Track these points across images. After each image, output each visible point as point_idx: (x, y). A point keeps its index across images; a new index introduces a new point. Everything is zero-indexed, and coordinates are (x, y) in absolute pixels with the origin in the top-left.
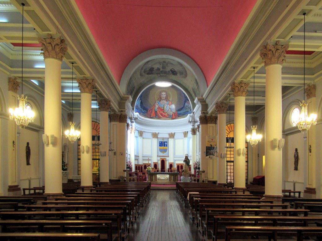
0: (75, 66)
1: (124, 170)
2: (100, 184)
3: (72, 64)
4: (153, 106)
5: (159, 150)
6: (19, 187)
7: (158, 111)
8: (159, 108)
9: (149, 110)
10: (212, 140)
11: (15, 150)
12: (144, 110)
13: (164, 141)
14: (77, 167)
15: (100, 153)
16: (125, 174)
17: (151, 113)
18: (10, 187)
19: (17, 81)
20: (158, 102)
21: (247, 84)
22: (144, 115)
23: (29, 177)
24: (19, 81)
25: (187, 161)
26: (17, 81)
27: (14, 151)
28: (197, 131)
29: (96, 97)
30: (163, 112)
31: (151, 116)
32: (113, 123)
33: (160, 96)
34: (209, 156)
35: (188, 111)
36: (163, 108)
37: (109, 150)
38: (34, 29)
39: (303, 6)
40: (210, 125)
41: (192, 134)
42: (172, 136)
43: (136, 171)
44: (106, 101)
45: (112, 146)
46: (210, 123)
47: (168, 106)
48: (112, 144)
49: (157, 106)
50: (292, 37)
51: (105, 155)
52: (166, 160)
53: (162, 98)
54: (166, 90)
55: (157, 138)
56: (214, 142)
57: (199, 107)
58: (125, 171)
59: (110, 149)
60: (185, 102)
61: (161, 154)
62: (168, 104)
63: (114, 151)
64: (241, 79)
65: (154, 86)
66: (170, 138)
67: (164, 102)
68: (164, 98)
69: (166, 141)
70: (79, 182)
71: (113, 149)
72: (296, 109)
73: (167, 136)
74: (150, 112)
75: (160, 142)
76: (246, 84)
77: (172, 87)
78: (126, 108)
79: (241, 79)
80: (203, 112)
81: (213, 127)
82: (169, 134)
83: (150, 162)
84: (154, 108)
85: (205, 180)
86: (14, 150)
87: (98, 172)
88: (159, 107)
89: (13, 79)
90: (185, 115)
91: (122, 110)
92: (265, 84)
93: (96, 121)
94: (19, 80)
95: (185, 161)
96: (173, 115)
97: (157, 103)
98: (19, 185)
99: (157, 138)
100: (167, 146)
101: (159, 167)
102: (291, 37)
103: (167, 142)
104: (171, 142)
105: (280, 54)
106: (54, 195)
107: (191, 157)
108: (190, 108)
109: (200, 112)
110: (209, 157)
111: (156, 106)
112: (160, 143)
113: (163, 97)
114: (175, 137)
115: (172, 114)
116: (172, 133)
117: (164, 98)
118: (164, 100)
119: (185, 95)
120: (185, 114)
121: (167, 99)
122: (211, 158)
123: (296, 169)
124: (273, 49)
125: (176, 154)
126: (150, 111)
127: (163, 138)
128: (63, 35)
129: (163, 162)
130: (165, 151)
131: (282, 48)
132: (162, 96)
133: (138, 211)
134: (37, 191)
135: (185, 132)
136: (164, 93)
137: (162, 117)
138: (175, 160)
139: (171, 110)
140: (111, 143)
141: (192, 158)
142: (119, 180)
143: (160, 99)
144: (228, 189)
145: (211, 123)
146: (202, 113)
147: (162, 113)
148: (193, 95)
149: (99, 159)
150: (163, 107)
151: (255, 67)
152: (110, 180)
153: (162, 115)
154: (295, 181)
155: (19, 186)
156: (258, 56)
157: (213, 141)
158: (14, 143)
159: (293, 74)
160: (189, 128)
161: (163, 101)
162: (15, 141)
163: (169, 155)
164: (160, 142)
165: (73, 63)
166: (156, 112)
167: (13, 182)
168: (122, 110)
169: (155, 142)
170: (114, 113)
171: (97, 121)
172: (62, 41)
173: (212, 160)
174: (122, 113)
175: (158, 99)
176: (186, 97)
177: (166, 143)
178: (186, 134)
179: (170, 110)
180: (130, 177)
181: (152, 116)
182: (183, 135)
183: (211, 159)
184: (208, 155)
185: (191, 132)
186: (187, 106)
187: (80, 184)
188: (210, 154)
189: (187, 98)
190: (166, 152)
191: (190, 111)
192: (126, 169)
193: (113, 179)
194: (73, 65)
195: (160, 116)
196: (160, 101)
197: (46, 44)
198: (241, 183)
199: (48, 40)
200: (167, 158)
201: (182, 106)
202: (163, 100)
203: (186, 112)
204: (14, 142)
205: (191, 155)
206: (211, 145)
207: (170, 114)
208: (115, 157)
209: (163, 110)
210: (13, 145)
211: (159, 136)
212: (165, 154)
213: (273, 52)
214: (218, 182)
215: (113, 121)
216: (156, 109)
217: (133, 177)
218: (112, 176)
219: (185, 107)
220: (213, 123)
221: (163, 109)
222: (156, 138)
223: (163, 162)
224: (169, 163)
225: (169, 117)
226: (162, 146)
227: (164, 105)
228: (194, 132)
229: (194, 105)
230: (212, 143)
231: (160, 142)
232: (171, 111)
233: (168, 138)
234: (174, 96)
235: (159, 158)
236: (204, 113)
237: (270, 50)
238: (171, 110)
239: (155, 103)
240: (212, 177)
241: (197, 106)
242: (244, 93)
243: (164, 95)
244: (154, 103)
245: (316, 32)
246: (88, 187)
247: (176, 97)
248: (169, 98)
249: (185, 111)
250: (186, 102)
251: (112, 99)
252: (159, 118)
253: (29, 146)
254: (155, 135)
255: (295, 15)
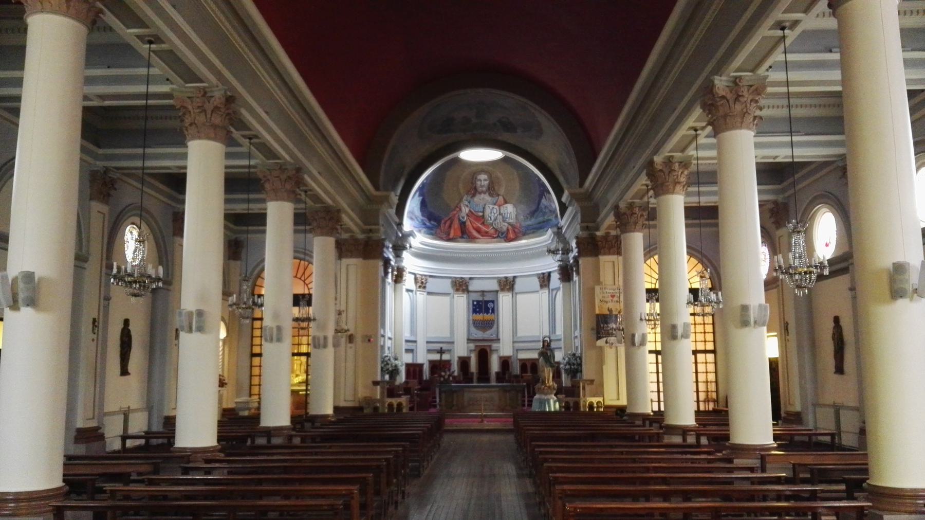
0: (256, 143)
1: (375, 380)
2: (313, 419)
3: (248, 140)
4: (454, 210)
5: (471, 322)
6: (99, 431)
7: (468, 223)
8: (471, 214)
9: (443, 222)
10: (613, 296)
11: (97, 343)
12: (430, 220)
13: (486, 299)
14: (247, 376)
15: (310, 338)
16: (378, 392)
17: (450, 227)
18: (79, 431)
19: (110, 177)
20: (469, 198)
21: (685, 164)
22: (432, 234)
23: (125, 406)
24: (115, 177)
25: (547, 353)
26: (110, 175)
27: (95, 341)
28: (574, 273)
29: (306, 203)
30: (483, 223)
31: (449, 235)
32: (345, 261)
33: (472, 183)
34: (605, 339)
35: (551, 220)
36: (481, 214)
37: (337, 331)
38: (168, 80)
39: (778, 14)
40: (606, 260)
41: (560, 279)
42: (508, 284)
43: (406, 382)
44: (329, 211)
45: (344, 320)
46: (605, 254)
47: (496, 207)
48: (344, 315)
49: (465, 210)
50: (770, 67)
51: (325, 346)
52: (491, 351)
53: (480, 189)
54: (490, 168)
55: (468, 291)
56: (617, 301)
57: (576, 213)
58: (376, 383)
59: (339, 328)
60: (541, 196)
61: (478, 334)
62: (495, 204)
63: (349, 333)
64: (670, 151)
65: (457, 161)
66: (502, 290)
67: (483, 199)
68: (484, 189)
69: (491, 299)
70: (256, 418)
71: (346, 328)
72: (826, 214)
73: (494, 286)
74: (447, 224)
75: (473, 301)
76: (683, 164)
77: (505, 160)
78: (381, 222)
79: (670, 151)
80: (586, 224)
81: (614, 262)
82: (500, 281)
83: (446, 357)
84: (457, 215)
85: (595, 405)
86: (93, 340)
87: (304, 388)
88: (470, 211)
89: (102, 172)
90: (542, 230)
91: (373, 227)
92: (655, 206)
93: (302, 256)
94: (115, 175)
95: (542, 354)
96: (508, 230)
97: (466, 203)
98: (101, 426)
99: (468, 291)
100: (493, 311)
101: (473, 366)
102: (768, 67)
103: (493, 302)
104: (504, 300)
105: (746, 106)
106: (196, 451)
107: (560, 340)
108: (554, 211)
109: (578, 227)
110: (607, 342)
111: (463, 208)
112: (474, 305)
113: (482, 186)
114: (517, 287)
115: (505, 229)
116: (506, 278)
117: (484, 189)
118: (485, 193)
119: (539, 179)
120: (541, 228)
121: (492, 190)
122: (612, 344)
123: (840, 370)
124: (729, 96)
125: (520, 334)
126: (445, 223)
127: (483, 292)
128: (232, 88)
129: (483, 355)
130: (487, 325)
131: (750, 92)
132: (479, 183)
133: (403, 489)
134: (154, 442)
135: (543, 274)
136: (483, 177)
137: (480, 237)
138: (517, 350)
139: (503, 217)
140: (340, 313)
141: (562, 344)
142: (360, 409)
143: (473, 191)
144: (705, 429)
145: (609, 254)
146: (582, 229)
147: (479, 227)
148: (561, 179)
149: (308, 355)
150: (482, 210)
151: (698, 128)
152: (336, 409)
153: (478, 231)
154: (839, 401)
155: (100, 428)
156: (698, 111)
157: (615, 299)
158: (96, 324)
159: (806, 134)
160: (551, 264)
161: (482, 195)
162: (99, 318)
163: (501, 336)
164: (475, 303)
165: (250, 139)
166: (463, 225)
167: (87, 419)
168: (373, 227)
169: (462, 302)
170: (352, 236)
171: (307, 258)
172: (230, 100)
173: (614, 349)
174: (371, 235)
175: (469, 191)
176: (543, 185)
177: (490, 305)
178: (545, 280)
179: (500, 217)
180: (389, 400)
181: (452, 235)
182: (536, 282)
183: (611, 348)
184: (603, 337)
185: (559, 274)
186: (546, 207)
187: (259, 422)
188: (609, 334)
189: (545, 186)
190: (491, 327)
191: (554, 220)
192: (379, 378)
193: (342, 404)
194: (252, 141)
195: (475, 234)
196: (474, 195)
197: (193, 109)
198: (686, 417)
199: (198, 100)
200: (494, 346)
201: (534, 208)
202: (480, 193)
203: (544, 222)
204: (94, 321)
205: (561, 335)
206: (608, 309)
207: (501, 228)
208: (351, 348)
209: (482, 219)
210: (93, 329)
211: (471, 288)
212: (488, 334)
213: (728, 101)
214: (628, 411)
215: (347, 257)
216: (463, 218)
217: (399, 400)
218: (342, 398)
219: (541, 211)
220: (613, 254)
221: (483, 216)
222: (463, 291)
223: (483, 355)
224: (500, 358)
225: (498, 237)
226: (479, 312)
227: (485, 205)
228: (566, 273)
229: (563, 208)
230: (611, 305)
231: (473, 301)
232: (504, 221)
233: (497, 292)
234: (510, 183)
235: (472, 346)
236: (587, 227)
237: (723, 97)
238: (503, 217)
239: (461, 200)
240: (615, 396)
241: (570, 209)
242: (678, 188)
243: (485, 180)
244: (457, 202)
245: (831, 51)
246: (279, 429)
247: (517, 185)
248: (496, 188)
249: (541, 219)
250: (542, 198)
251: (344, 204)
252: (471, 239)
253: (130, 328)
254: (461, 285)
255: (765, 31)
